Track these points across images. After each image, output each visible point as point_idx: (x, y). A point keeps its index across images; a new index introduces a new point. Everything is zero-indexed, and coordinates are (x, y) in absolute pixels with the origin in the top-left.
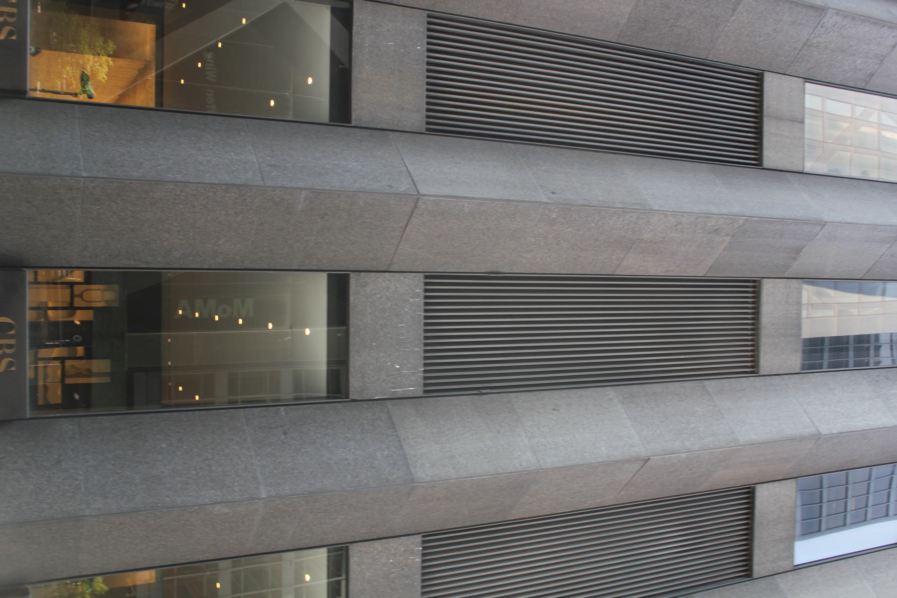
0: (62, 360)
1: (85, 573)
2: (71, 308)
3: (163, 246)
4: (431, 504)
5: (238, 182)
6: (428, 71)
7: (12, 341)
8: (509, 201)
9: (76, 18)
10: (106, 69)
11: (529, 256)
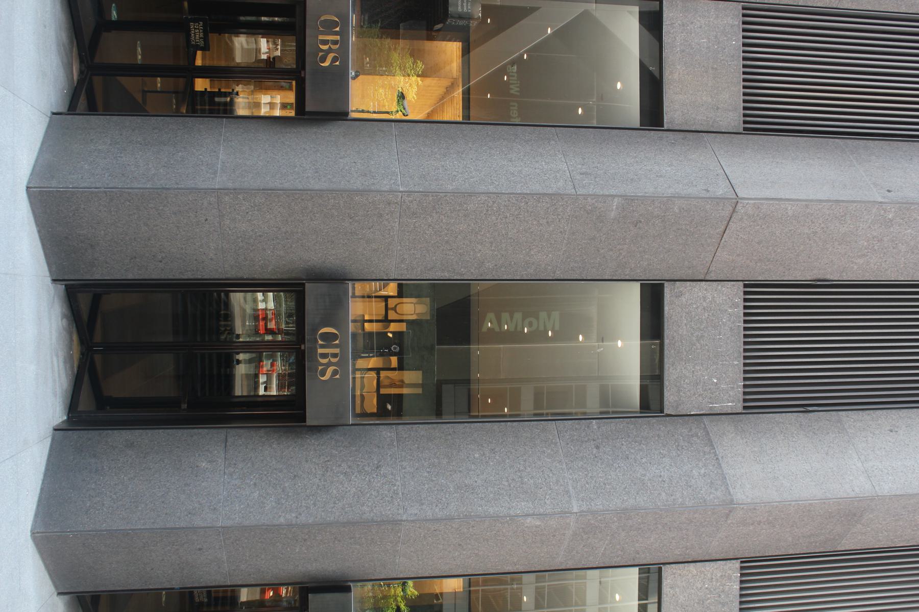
0: (378, 370)
1: (401, 576)
2: (386, 320)
3: (469, 258)
4: (751, 528)
5: (550, 191)
6: (744, 66)
7: (337, 351)
8: (837, 201)
9: (388, 42)
10: (415, 89)
11: (861, 261)
